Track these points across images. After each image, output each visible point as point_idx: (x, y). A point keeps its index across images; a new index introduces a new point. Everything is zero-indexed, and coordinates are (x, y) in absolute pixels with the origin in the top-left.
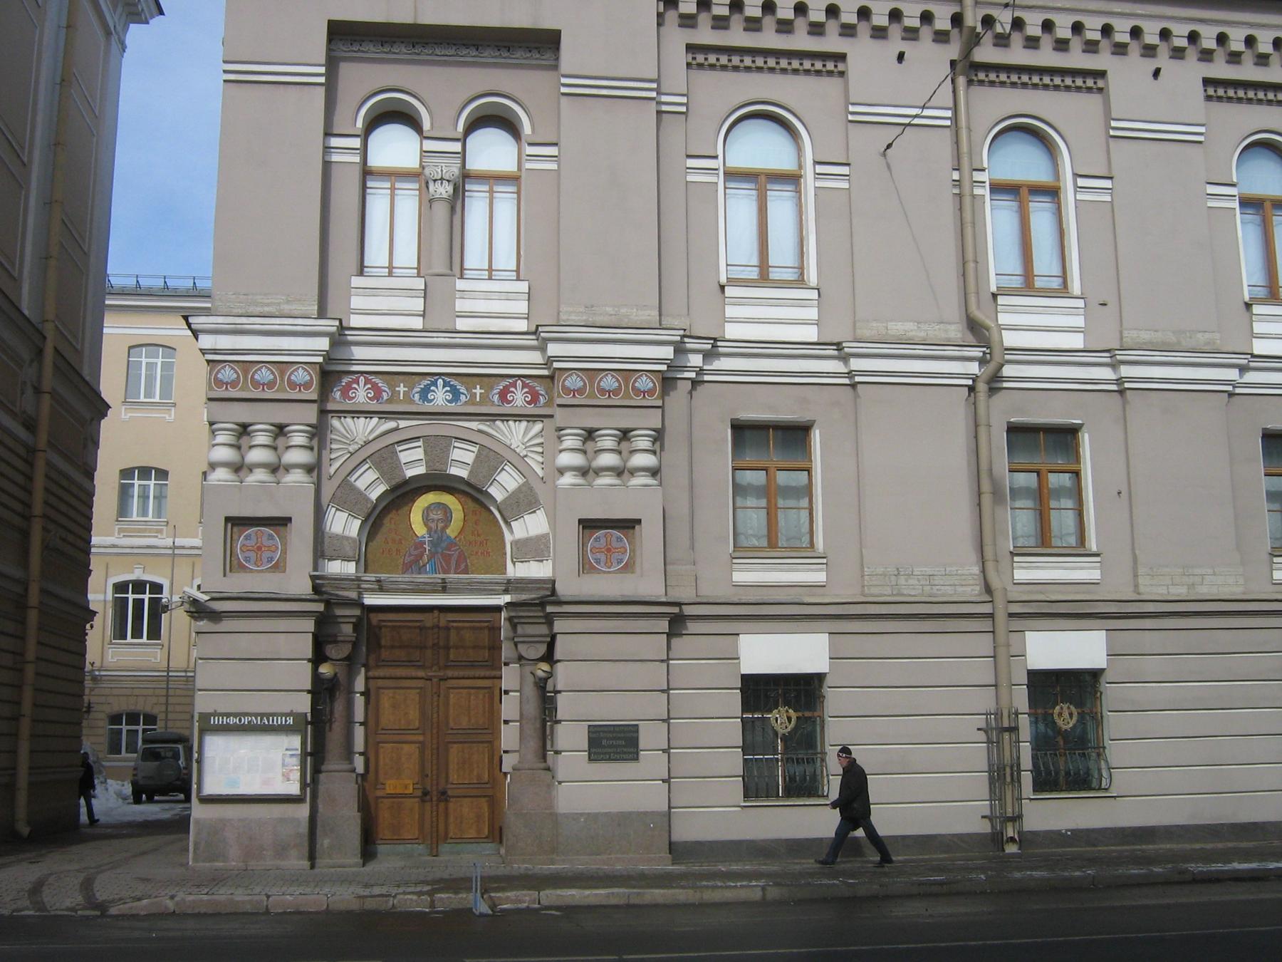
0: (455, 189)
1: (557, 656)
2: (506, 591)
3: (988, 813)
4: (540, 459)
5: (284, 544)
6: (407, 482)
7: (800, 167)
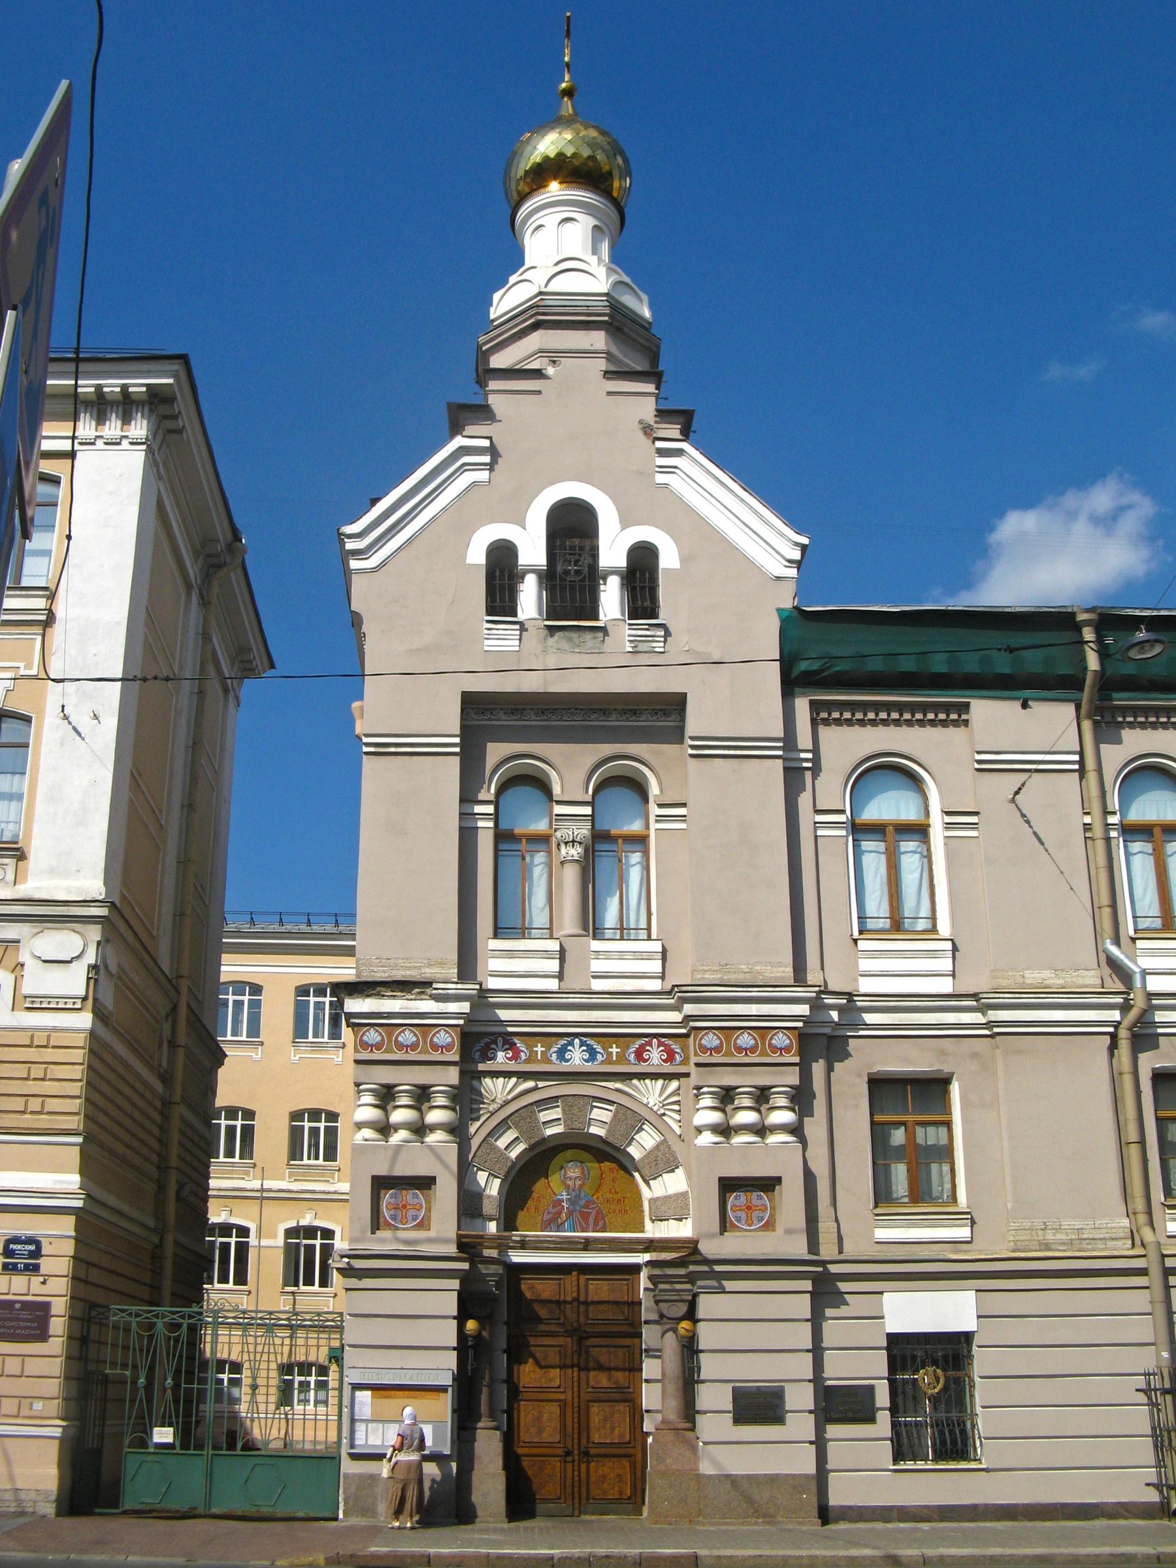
0: (586, 851)
1: (701, 1314)
2: (646, 1250)
3: (1155, 1480)
4: (677, 1117)
5: (428, 1202)
6: (544, 1140)
7: (927, 814)
